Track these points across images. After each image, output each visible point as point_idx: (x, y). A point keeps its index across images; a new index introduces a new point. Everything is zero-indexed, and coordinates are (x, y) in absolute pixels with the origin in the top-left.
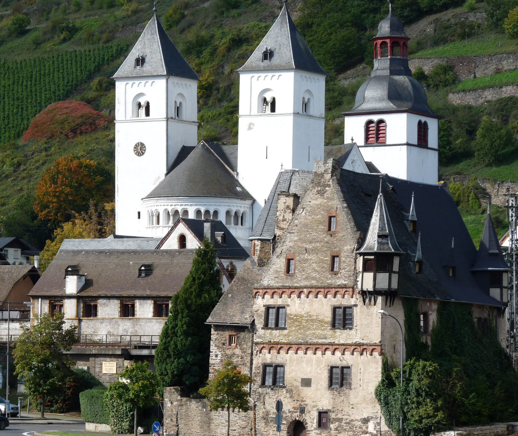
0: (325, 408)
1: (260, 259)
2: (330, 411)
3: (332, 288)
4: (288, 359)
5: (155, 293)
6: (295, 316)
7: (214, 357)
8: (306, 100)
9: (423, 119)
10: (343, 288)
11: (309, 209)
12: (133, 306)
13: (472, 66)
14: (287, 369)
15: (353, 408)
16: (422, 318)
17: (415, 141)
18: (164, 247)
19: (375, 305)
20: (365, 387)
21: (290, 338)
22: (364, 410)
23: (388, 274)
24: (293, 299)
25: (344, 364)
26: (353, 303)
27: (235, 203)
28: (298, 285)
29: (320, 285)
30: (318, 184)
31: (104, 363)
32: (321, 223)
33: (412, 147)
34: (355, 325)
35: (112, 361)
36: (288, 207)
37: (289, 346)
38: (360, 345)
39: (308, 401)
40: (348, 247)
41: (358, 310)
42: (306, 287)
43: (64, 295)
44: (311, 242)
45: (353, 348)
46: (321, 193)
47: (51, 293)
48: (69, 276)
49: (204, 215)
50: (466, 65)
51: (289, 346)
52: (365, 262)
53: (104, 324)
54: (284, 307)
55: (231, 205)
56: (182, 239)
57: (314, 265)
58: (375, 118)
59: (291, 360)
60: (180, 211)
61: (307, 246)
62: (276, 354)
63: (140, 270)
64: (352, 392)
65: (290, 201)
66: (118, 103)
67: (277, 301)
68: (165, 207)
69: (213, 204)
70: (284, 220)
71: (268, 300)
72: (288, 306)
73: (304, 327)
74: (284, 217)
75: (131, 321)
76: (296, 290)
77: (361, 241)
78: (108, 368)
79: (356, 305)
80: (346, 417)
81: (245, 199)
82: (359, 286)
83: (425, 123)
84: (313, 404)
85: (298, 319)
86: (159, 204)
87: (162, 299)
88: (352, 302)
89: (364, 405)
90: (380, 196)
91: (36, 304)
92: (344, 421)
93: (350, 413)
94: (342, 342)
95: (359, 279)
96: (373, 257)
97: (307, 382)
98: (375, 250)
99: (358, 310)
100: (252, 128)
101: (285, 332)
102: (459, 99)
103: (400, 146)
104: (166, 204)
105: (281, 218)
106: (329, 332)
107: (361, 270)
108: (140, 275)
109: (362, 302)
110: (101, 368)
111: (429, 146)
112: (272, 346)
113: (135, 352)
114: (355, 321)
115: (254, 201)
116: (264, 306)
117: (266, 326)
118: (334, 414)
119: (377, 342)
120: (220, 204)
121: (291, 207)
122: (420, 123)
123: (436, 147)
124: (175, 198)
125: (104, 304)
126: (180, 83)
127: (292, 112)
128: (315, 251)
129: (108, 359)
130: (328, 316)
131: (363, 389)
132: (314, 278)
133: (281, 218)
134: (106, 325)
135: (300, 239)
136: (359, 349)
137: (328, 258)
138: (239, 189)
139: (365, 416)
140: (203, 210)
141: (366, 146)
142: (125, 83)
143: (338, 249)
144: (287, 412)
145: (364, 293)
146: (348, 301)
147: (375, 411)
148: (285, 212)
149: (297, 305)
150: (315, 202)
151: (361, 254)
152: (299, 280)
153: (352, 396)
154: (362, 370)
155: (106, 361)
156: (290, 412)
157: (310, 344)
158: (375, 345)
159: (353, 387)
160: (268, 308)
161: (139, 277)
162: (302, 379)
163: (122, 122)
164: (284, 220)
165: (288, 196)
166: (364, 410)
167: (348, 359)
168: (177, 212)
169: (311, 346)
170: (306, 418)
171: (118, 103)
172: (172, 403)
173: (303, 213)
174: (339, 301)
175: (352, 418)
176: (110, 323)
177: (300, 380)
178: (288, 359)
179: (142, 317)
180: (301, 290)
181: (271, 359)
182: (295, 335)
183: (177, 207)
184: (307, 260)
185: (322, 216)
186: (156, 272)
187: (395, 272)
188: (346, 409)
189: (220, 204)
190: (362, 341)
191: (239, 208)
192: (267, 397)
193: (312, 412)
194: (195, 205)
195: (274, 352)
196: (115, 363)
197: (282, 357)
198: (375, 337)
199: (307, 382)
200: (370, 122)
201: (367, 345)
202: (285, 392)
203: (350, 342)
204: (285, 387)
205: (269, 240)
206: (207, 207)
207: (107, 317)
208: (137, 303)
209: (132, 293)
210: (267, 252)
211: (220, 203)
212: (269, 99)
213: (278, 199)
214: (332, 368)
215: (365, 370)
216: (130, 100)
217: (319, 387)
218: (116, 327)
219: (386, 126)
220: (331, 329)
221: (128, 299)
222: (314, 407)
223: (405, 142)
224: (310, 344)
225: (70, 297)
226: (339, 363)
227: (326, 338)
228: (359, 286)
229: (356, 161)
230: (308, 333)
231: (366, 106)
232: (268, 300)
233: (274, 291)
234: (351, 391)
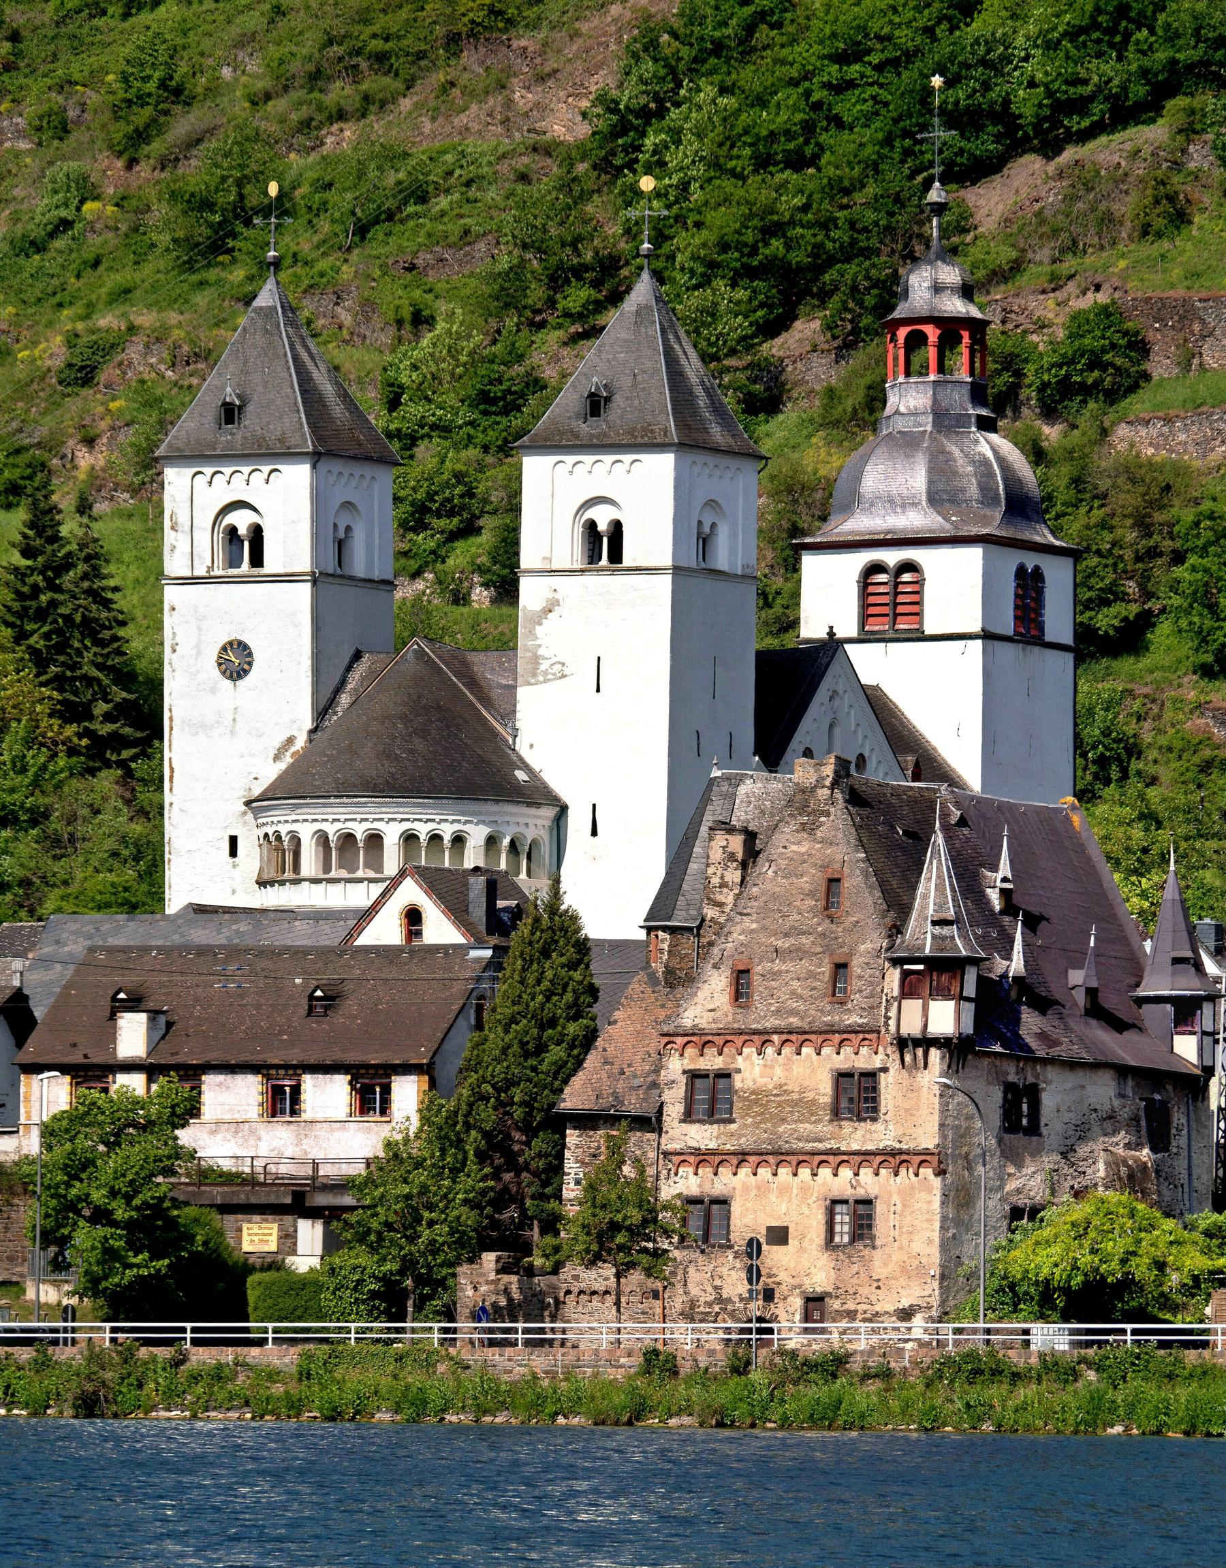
0: (819, 1290)
1: (669, 971)
2: (829, 1294)
3: (834, 1032)
4: (738, 1187)
5: (354, 1057)
6: (753, 1093)
7: (572, 1186)
8: (707, 529)
9: (1031, 561)
10: (857, 1032)
11: (783, 863)
12: (296, 1090)
14: (736, 1208)
15: (878, 1288)
16: (1025, 1107)
17: (1008, 628)
18: (365, 939)
19: (925, 1067)
20: (905, 1243)
21: (743, 1140)
22: (903, 1292)
24: (749, 1057)
25: (861, 1193)
26: (878, 1065)
27: (512, 814)
28: (759, 1027)
29: (807, 1027)
30: (803, 809)
31: (245, 1226)
32: (811, 894)
33: (998, 645)
34: (883, 1110)
35: (266, 1221)
36: (731, 857)
37: (742, 1156)
38: (893, 1153)
39: (782, 1276)
40: (869, 945)
41: (891, 1080)
42: (777, 1031)
43: (111, 1062)
44: (786, 935)
45: (879, 1159)
46: (809, 829)
48: (125, 1015)
50: (1173, 327)
51: (742, 1156)
52: (905, 975)
53: (219, 1137)
54: (728, 1076)
55: (500, 820)
56: (413, 917)
57: (795, 983)
58: (892, 557)
59: (746, 1188)
60: (359, 837)
61: (779, 943)
62: (711, 1175)
63: (311, 997)
64: (877, 1254)
65: (736, 844)
67: (712, 1062)
68: (317, 826)
70: (723, 885)
71: (692, 1060)
72: (738, 1071)
73: (772, 1116)
74: (722, 877)
75: (293, 1127)
76: (755, 1038)
77: (896, 930)
78: (256, 1238)
79: (885, 1070)
80: (865, 1307)
81: (538, 805)
82: (892, 1028)
83: (1038, 574)
84: (793, 1281)
85: (758, 1097)
86: (301, 817)
88: (877, 1061)
89: (903, 1282)
90: (939, 839)
92: (860, 1317)
93: (873, 1298)
94: (855, 1147)
95: (893, 1013)
96: (921, 967)
97: (779, 1236)
98: (927, 951)
99: (891, 1080)
101: (733, 1127)
102: (1150, 444)
103: (961, 643)
105: (716, 881)
106: (825, 1128)
107: (896, 993)
108: (311, 1010)
109: (898, 1062)
110: (240, 1238)
111: (1048, 638)
112: (702, 1157)
113: (322, 1200)
114: (883, 1103)
116: (684, 1072)
117: (688, 1116)
118: (838, 1302)
119: (931, 1146)
121: (740, 856)
122: (1021, 572)
123: (1068, 640)
124: (345, 800)
125: (220, 1085)
126: (346, 472)
127: (668, 561)
128: (798, 953)
129: (257, 1218)
130: (824, 1089)
131: (901, 1248)
132: (793, 1012)
133: (716, 881)
134: (225, 1138)
135: (764, 928)
136: (894, 1161)
137: (826, 970)
138: (521, 775)
139: (905, 1303)
140: (423, 830)
141: (865, 638)
142: (190, 471)
143: (846, 949)
144: (736, 1299)
145: (902, 1043)
146: (865, 1059)
147: (927, 1293)
148: (726, 868)
149: (757, 1070)
150: (795, 848)
151: (896, 962)
152: (762, 1015)
153: (876, 1263)
154: (899, 1207)
155: (250, 1222)
156: (741, 1300)
157: (787, 1154)
158: (926, 1152)
159: (878, 1242)
160: (694, 1076)
161: (309, 1015)
162: (769, 1229)
164: (723, 885)
165: (731, 830)
166: (903, 1292)
167: (869, 1182)
168: (349, 838)
169: (788, 1158)
170: (777, 1312)
171: (173, 528)
172: (475, 1288)
173: (770, 872)
174: (849, 1059)
175: (877, 1308)
176: (236, 1132)
177: (764, 1232)
178: (738, 1187)
179: (319, 1117)
180: (766, 1037)
181: (700, 1186)
182: (753, 1134)
184: (780, 972)
185: (811, 879)
186: (350, 1005)
187: (968, 999)
188: (864, 1291)
190: (898, 1146)
191: (522, 829)
192: (691, 1270)
193: (790, 1299)
195: (705, 1171)
196: (275, 1226)
197: (724, 1182)
198: (927, 1137)
199: (779, 1236)
200: (876, 568)
201: (907, 1153)
202: (731, 1258)
203: (871, 1147)
204: (731, 1247)
205: (690, 929)
207: (227, 1117)
208: (309, 1082)
209: (294, 1057)
210: (686, 955)
213: (711, 839)
214: (835, 1202)
215: (904, 1206)
216: (205, 519)
217: (805, 1245)
218: (252, 1142)
219: (920, 583)
220: (831, 1121)
221: (282, 1072)
222: (795, 1287)
223: (976, 626)
224: (787, 1154)
226: (848, 1193)
227: (820, 1141)
228: (892, 1028)
229: (841, 692)
230: (781, 1130)
231: (859, 523)
232: (692, 1060)
233: (702, 1039)
234: (874, 1252)
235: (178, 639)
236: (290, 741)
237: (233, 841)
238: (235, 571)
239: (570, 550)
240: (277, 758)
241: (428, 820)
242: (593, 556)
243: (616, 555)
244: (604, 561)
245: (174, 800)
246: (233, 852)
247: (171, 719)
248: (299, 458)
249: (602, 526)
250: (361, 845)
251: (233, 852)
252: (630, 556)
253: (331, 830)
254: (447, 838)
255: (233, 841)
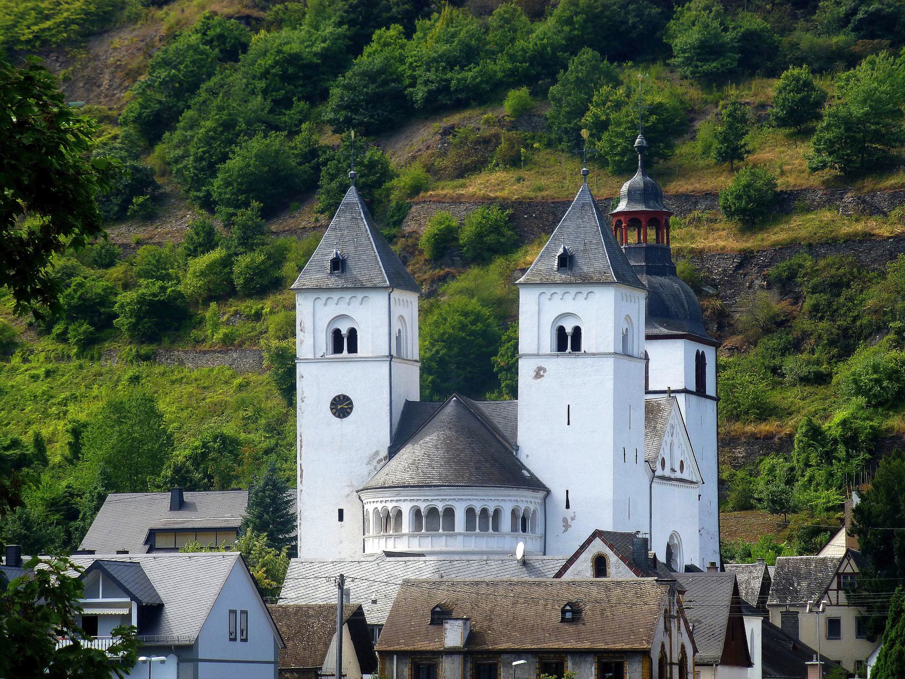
9: (702, 348)
13: (547, 220)
23: (199, 663)
47: (416, 647)
49: (427, 517)
50: (535, 218)
66: (301, 330)
69: (493, 498)
87: (611, 655)
91: (388, 665)
100: (542, 376)
104: (384, 499)
115: (548, 492)
120: (503, 498)
163: (307, 361)
171: (301, 330)
183: (434, 503)
189: (503, 498)
194: (411, 500)
206: (483, 503)
211: (505, 496)
212: (569, 330)
221: (553, 655)
225: (451, 652)
235: (305, 395)
236: (377, 453)
237: (341, 512)
238: (338, 355)
239: (548, 342)
240: (369, 463)
241: (411, 500)
242: (338, 349)
243: (576, 346)
244: (569, 349)
245: (304, 489)
246: (341, 518)
247: (301, 441)
248: (529, 286)
249: (344, 331)
250: (441, 514)
251: (341, 518)
252: (585, 345)
253: (423, 506)
254: (478, 511)
255: (341, 512)
